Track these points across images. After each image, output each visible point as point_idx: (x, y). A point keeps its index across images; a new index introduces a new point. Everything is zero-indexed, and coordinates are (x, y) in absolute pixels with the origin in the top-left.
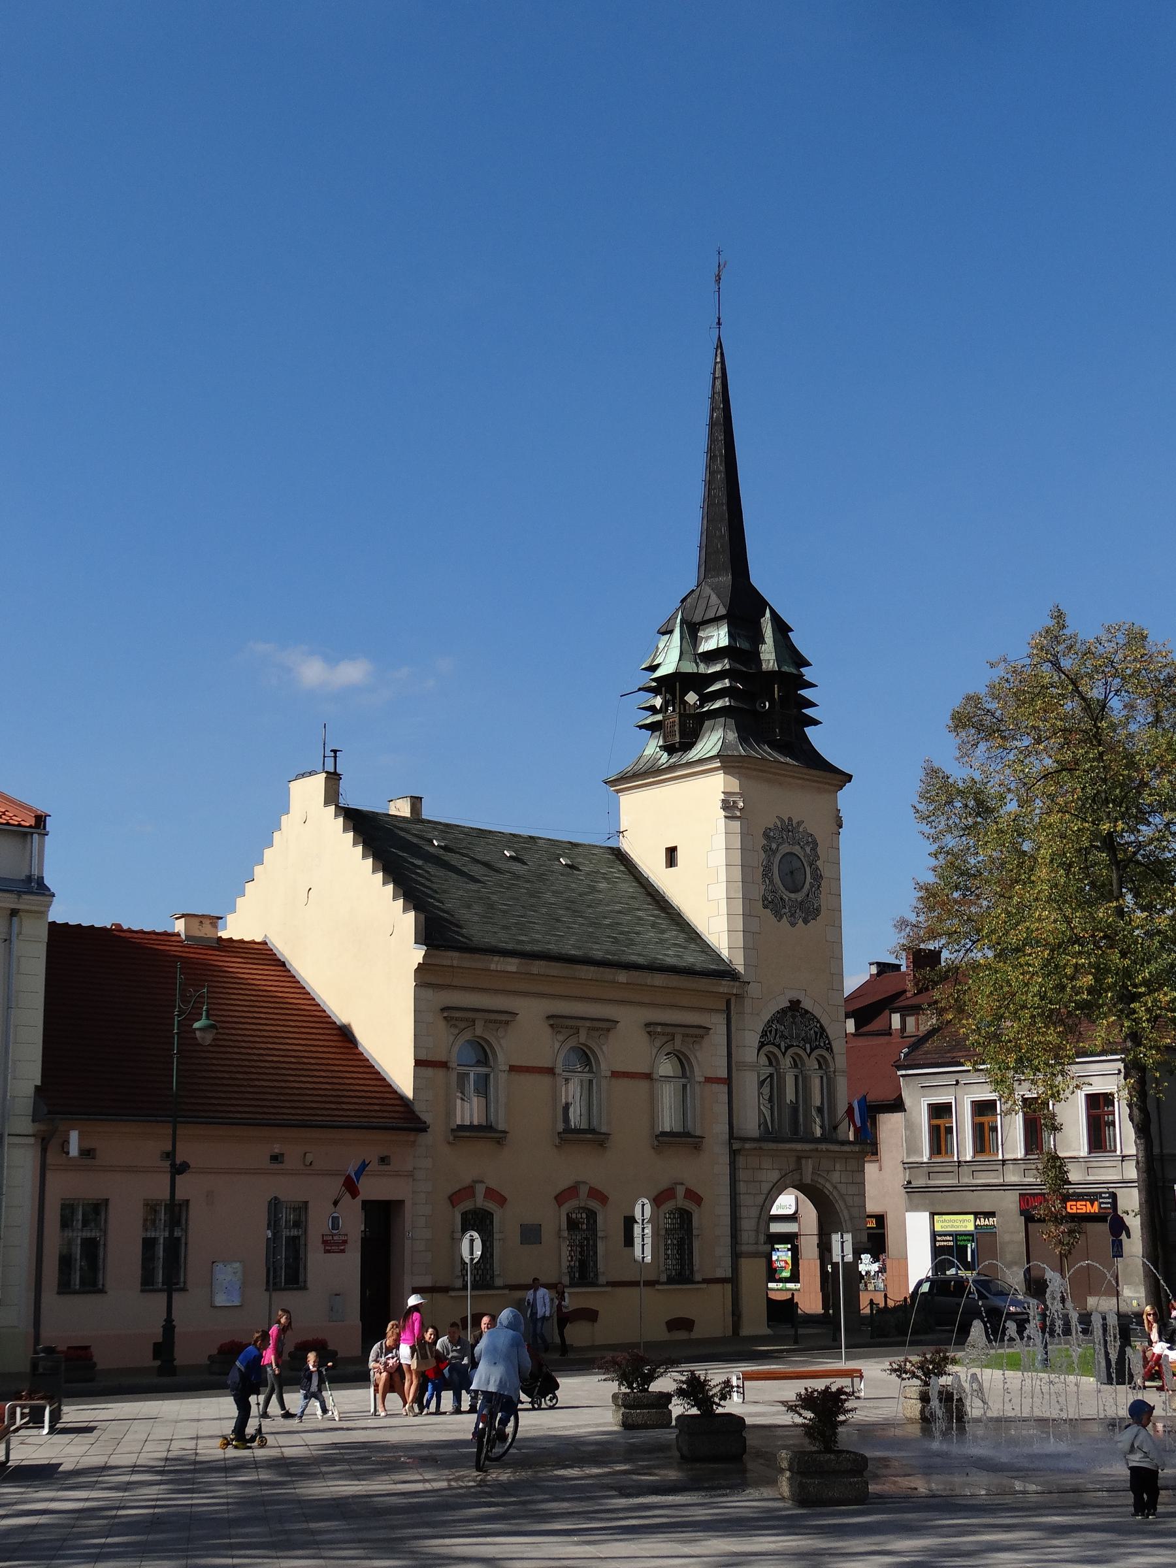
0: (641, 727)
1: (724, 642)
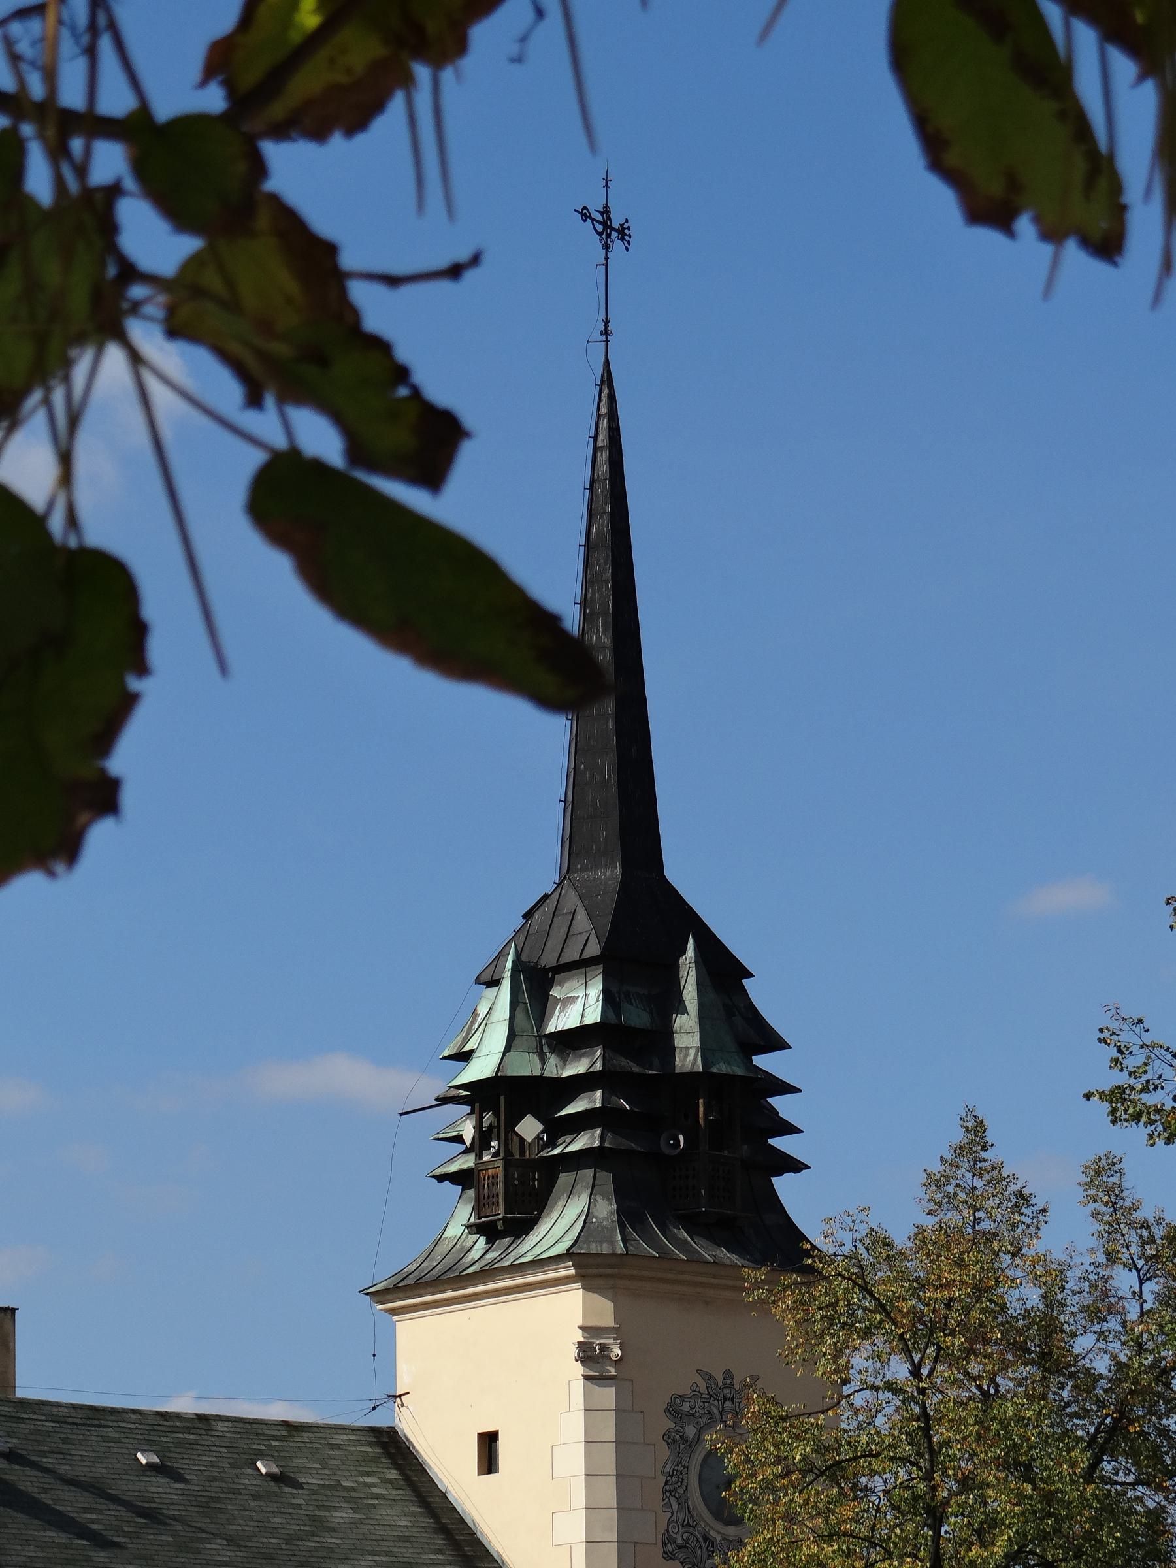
0: (441, 1178)
1: (594, 1016)
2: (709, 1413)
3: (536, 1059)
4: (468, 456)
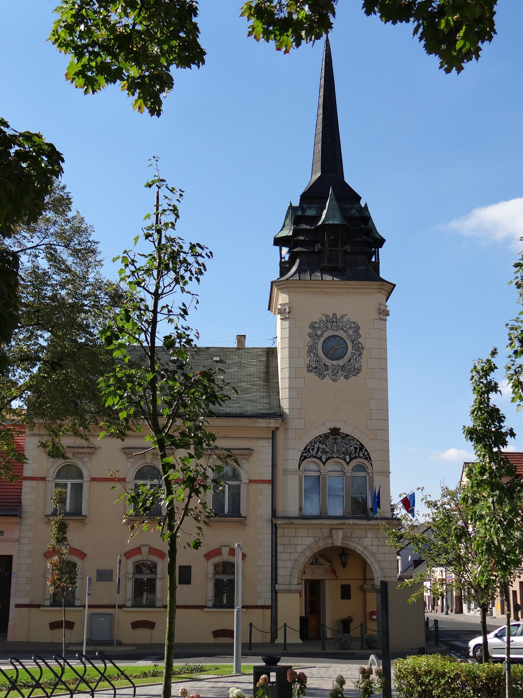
4: (48, 628)
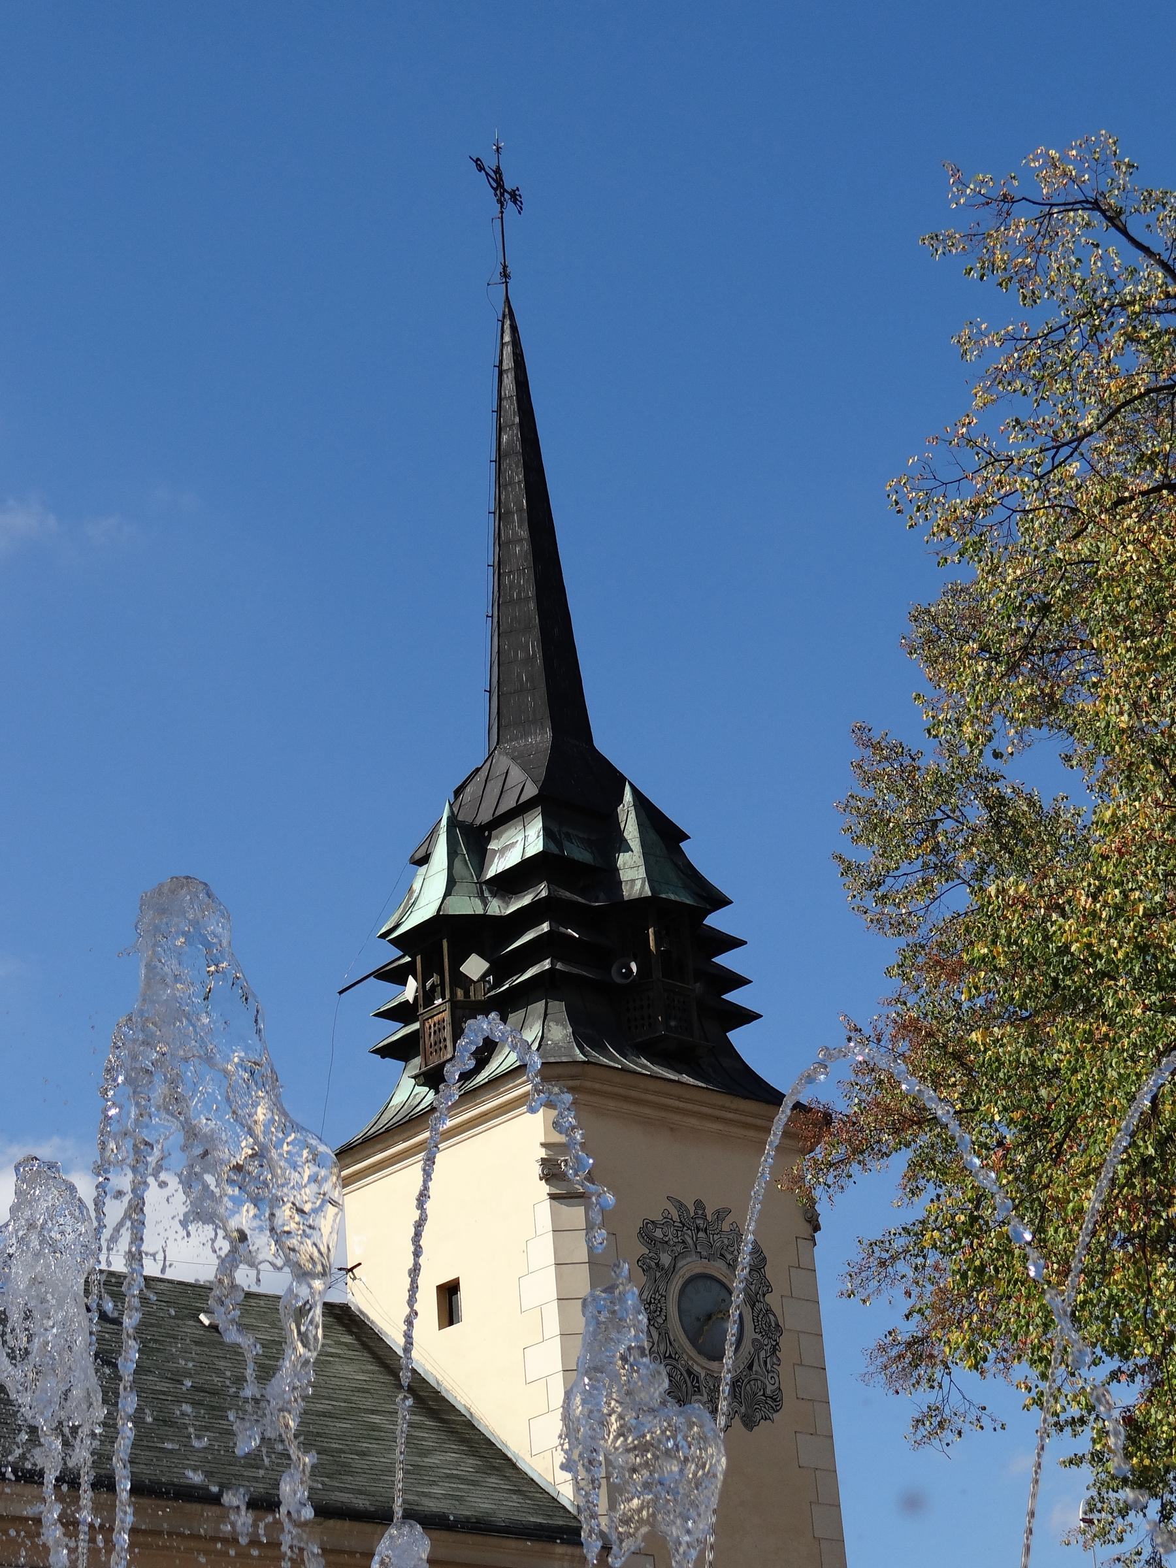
2: (683, 1242)
3: (478, 902)
